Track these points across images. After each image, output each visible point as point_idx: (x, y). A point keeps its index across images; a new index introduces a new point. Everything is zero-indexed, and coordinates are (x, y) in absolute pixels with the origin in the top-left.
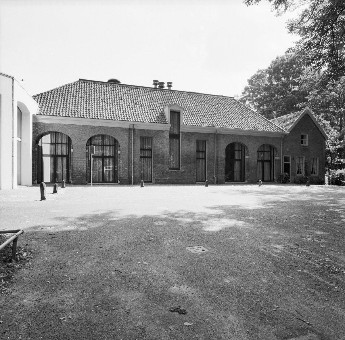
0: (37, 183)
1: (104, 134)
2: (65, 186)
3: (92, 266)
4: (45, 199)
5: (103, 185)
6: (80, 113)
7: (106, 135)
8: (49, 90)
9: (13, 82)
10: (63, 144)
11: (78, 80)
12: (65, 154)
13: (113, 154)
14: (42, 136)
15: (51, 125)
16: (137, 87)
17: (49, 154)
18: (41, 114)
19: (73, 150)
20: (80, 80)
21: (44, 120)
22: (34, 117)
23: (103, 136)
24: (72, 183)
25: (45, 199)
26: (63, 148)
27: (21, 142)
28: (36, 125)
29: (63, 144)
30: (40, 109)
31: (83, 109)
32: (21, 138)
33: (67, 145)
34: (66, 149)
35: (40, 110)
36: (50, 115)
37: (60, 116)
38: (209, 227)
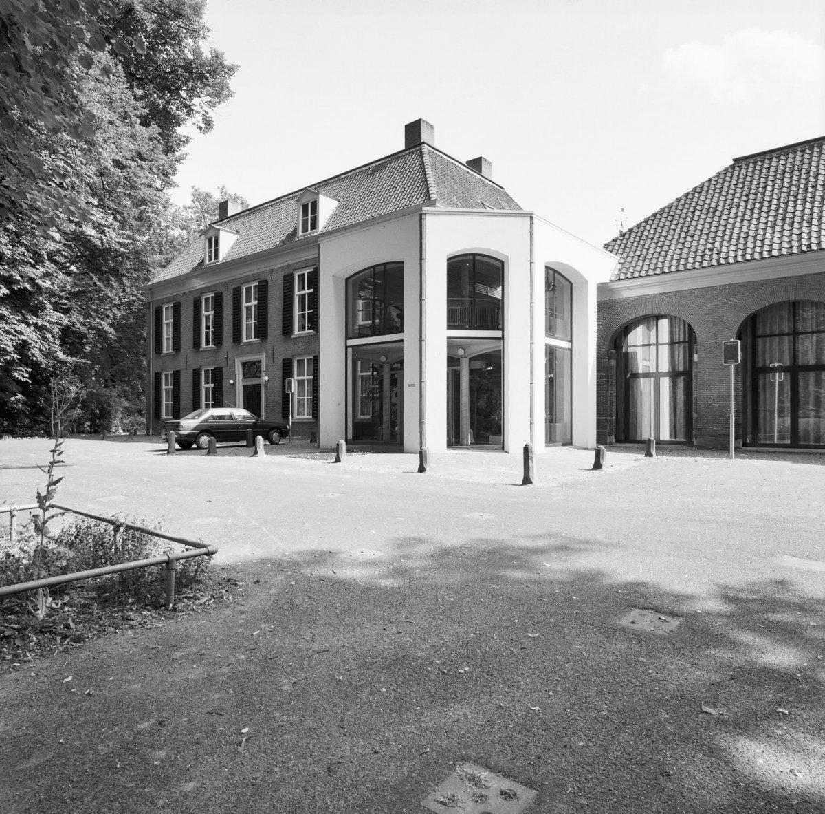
0: (614, 440)
1: (794, 298)
2: (653, 452)
3: (158, 622)
4: (531, 483)
5: (758, 452)
6: (719, 253)
7: (799, 302)
8: (657, 209)
9: (532, 224)
10: (676, 343)
11: (732, 162)
12: (681, 369)
13: (685, 367)
14: (627, 329)
15: (644, 300)
16: (793, 148)
17: (660, 371)
18: (619, 279)
19: (699, 358)
20: (736, 160)
21: (630, 291)
22: (602, 288)
23: (794, 306)
24: (695, 443)
25: (531, 483)
26: (676, 353)
27: (571, 350)
28: (606, 306)
29: (676, 343)
30: (620, 266)
31: (731, 239)
32: (571, 341)
33: (687, 344)
34: (684, 357)
35: (620, 270)
36: (656, 274)
37: (664, 273)
38: (195, 586)
